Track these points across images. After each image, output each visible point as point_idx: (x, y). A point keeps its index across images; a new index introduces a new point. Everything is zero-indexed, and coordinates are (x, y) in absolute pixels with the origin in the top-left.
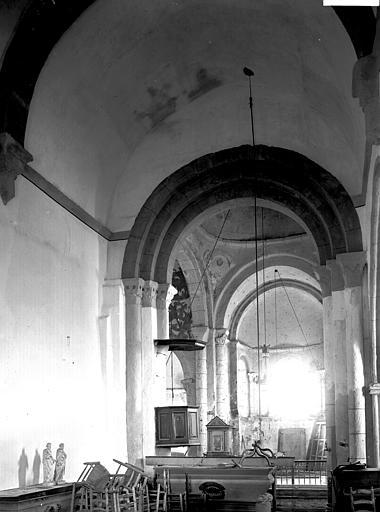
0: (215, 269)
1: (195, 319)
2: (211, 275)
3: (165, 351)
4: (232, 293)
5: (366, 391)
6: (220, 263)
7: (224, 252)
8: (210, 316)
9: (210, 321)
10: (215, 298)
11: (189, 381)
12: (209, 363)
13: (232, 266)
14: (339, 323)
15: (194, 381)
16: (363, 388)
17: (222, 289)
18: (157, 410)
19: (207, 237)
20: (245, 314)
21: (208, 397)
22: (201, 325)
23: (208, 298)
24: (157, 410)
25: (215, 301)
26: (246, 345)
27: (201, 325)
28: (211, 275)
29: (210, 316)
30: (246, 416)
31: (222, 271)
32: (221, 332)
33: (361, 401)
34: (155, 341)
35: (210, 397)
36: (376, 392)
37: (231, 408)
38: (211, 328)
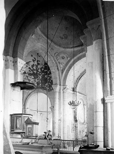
0: (62, 61)
1: (54, 83)
2: (59, 63)
3: (18, 89)
4: (69, 70)
5: (103, 101)
6: (63, 58)
7: (64, 53)
8: (60, 80)
9: (60, 83)
10: (62, 73)
11: (52, 107)
12: (60, 99)
13: (69, 59)
14: (90, 64)
15: (54, 107)
16: (102, 99)
17: (65, 69)
18: (11, 115)
19: (56, 46)
20: (80, 82)
21: (59, 113)
22: (56, 84)
23: (59, 73)
24: (11, 115)
25: (62, 74)
26: (82, 94)
27: (56, 84)
28: (59, 63)
29: (60, 80)
30: (83, 122)
31: (64, 62)
32: (64, 87)
33: (100, 107)
34: (11, 84)
35: (60, 113)
36: (109, 101)
37: (74, 119)
38: (60, 85)
